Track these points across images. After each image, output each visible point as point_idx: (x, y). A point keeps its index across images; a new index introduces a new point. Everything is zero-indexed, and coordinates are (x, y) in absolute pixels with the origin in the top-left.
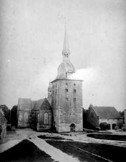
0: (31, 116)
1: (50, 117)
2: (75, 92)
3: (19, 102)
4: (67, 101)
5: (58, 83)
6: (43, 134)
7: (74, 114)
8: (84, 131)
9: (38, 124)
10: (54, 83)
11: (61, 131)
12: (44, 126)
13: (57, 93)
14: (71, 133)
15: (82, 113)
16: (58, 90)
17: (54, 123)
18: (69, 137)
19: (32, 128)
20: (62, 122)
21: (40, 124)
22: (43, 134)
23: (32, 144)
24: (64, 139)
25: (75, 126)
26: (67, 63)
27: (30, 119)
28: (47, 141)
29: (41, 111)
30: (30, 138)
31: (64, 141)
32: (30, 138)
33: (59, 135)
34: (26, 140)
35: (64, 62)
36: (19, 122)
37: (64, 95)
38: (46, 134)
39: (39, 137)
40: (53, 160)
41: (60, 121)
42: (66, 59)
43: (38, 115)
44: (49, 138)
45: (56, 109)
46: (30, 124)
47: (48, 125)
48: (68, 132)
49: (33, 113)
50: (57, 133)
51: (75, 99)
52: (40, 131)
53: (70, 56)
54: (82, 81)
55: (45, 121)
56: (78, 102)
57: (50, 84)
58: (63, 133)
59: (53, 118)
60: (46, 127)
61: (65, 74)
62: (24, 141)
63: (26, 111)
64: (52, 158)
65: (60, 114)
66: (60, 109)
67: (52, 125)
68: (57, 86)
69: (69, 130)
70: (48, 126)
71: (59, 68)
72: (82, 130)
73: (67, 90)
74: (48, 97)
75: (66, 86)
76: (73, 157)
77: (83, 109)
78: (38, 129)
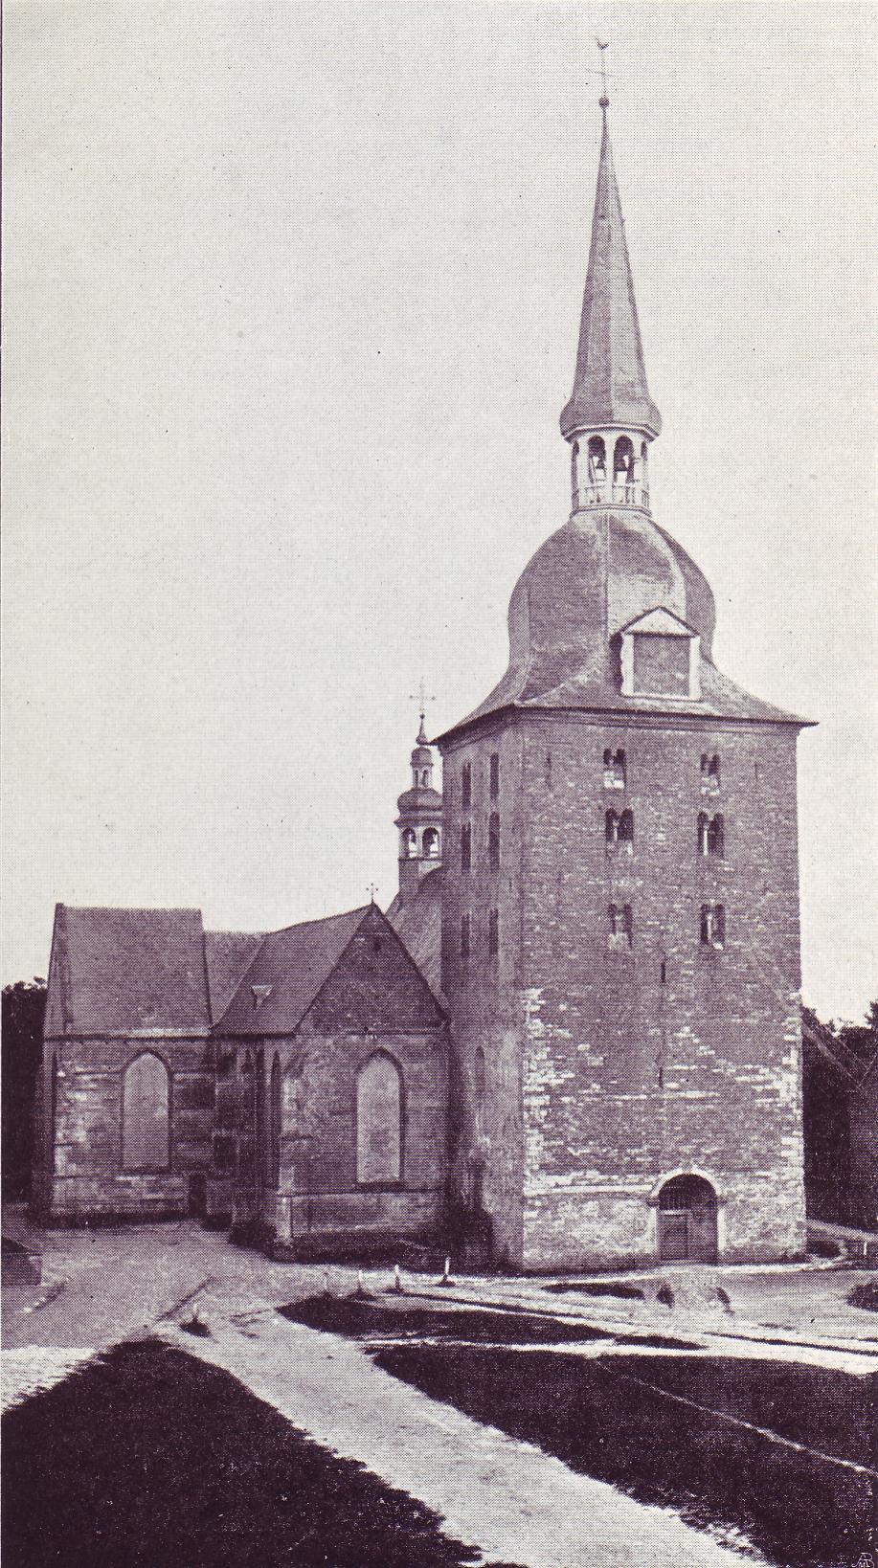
0: (198, 1096)
1: (427, 1103)
2: (716, 842)
3: (59, 952)
4: (617, 939)
5: (511, 743)
6: (344, 1279)
7: (706, 1076)
8: (822, 1248)
9: (287, 1183)
10: (468, 753)
11: (551, 1257)
12: (356, 1199)
13: (508, 859)
14: (665, 1272)
15: (793, 1059)
16: (520, 825)
17: (478, 1169)
18: (647, 1318)
19: (215, 1223)
20: (563, 1164)
21: (311, 1178)
22: (344, 1279)
23: (223, 1389)
24: (704, 1347)
25: (713, 1202)
26: (624, 536)
27: (180, 1133)
28: (385, 1360)
29: (317, 1045)
30: (197, 1328)
31: (591, 1349)
32: (197, 1328)
33: (533, 1297)
34: (153, 1345)
35: (586, 524)
36: (60, 1158)
37: (581, 876)
38: (375, 1280)
39: (292, 1312)
40: (471, 1553)
41: (535, 1145)
42: (609, 486)
43: (289, 1088)
44: (419, 1320)
45: (493, 1019)
46: (197, 1184)
47: (398, 1188)
48: (630, 1264)
49: (225, 1065)
50: (508, 1267)
51: (711, 923)
52: (306, 1253)
53: (657, 464)
54: (793, 726)
55: (362, 1149)
56: (748, 944)
57: (418, 759)
58: (563, 1274)
59: (454, 1122)
60: (369, 1215)
61: (599, 656)
62: (123, 1352)
63: (147, 1046)
64: (450, 1528)
65: (543, 1075)
66: (537, 1026)
67: (447, 1189)
68: (507, 781)
69: (647, 1244)
70: (396, 1203)
71: (511, 618)
72: (792, 1241)
73: (620, 824)
74: (400, 900)
75: (612, 781)
76: (697, 1522)
77: (809, 1018)
78: (285, 1232)
